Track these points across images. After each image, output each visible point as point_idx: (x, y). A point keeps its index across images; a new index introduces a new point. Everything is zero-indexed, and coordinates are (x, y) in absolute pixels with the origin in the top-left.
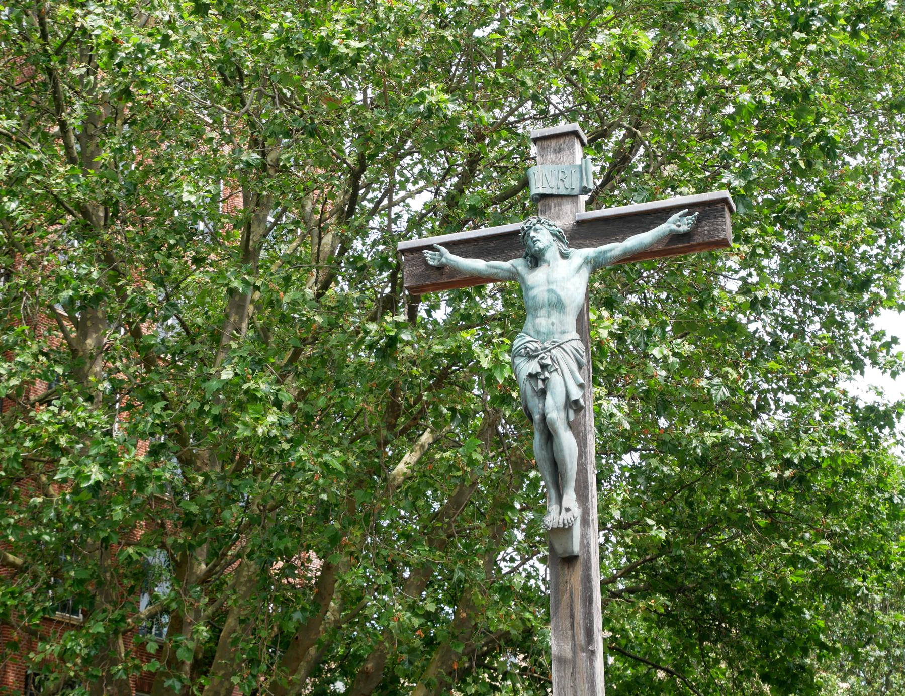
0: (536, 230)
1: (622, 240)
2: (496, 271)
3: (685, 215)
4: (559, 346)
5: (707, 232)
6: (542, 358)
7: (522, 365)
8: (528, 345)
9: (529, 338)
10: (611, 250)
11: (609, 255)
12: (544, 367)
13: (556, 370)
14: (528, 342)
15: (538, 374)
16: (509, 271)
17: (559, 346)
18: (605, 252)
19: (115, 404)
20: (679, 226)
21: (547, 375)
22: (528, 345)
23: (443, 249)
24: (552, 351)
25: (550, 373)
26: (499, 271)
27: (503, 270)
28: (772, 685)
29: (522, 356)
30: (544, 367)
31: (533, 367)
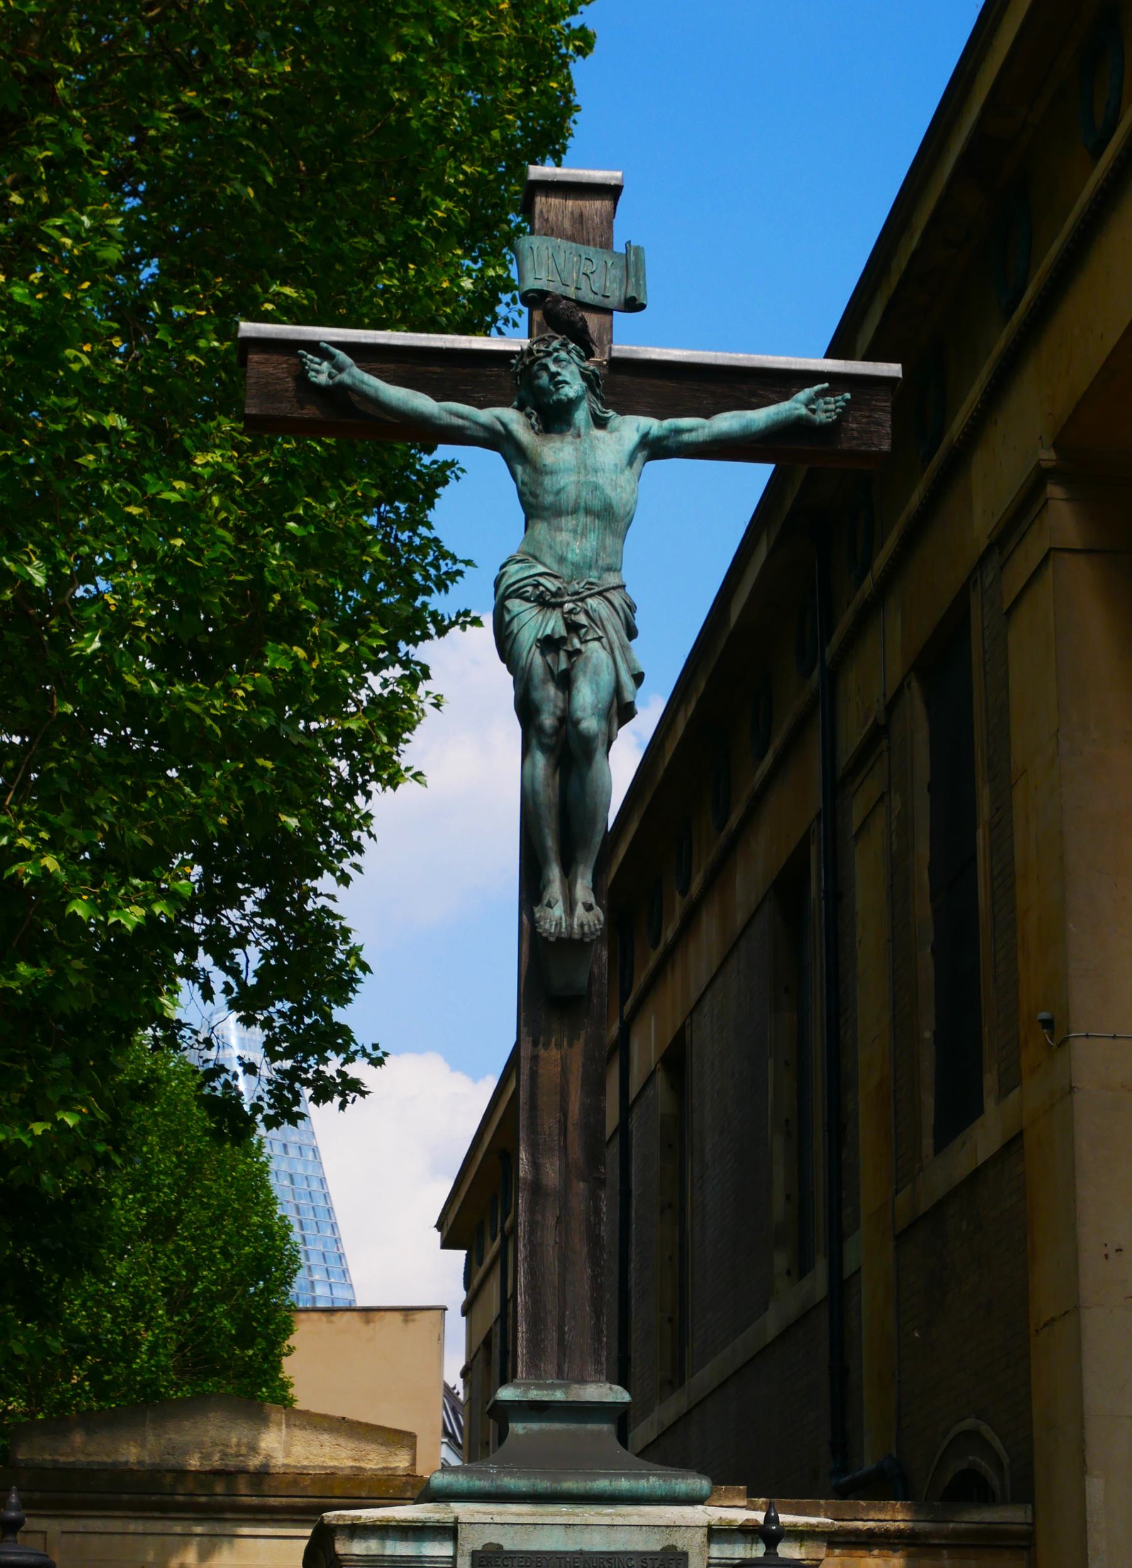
0: (557, 361)
1: (707, 414)
2: (460, 422)
3: (821, 394)
4: (600, 593)
5: (856, 434)
6: (571, 612)
7: (525, 617)
8: (542, 580)
9: (540, 569)
10: (690, 430)
11: (686, 437)
12: (573, 627)
13: (599, 639)
14: (541, 575)
15: (563, 640)
16: (485, 427)
17: (600, 593)
18: (678, 431)
19: (306, 649)
20: (813, 411)
21: (576, 643)
22: (542, 580)
23: (341, 355)
24: (589, 601)
25: (584, 642)
26: (466, 423)
27: (476, 423)
28: (162, 1015)
29: (527, 600)
30: (573, 627)
31: (553, 624)
